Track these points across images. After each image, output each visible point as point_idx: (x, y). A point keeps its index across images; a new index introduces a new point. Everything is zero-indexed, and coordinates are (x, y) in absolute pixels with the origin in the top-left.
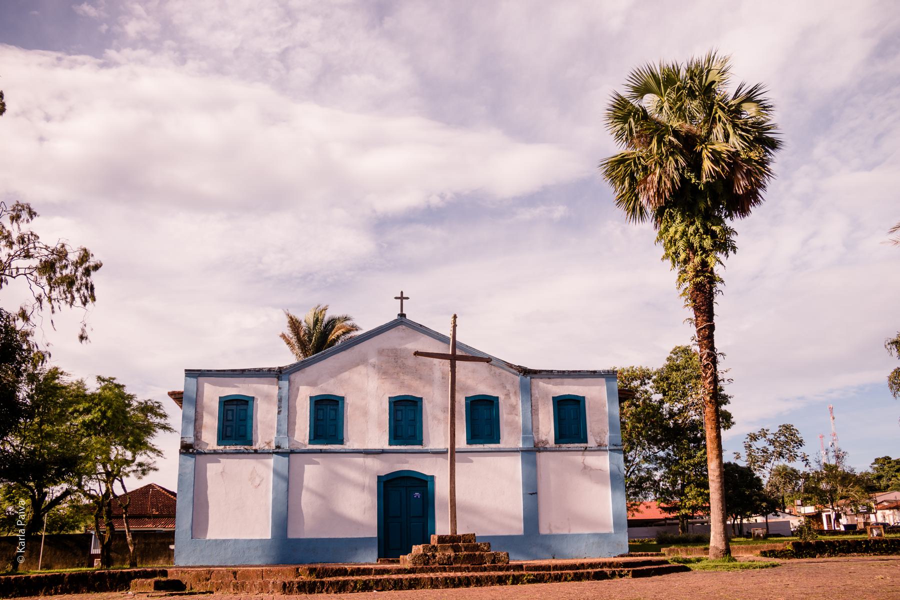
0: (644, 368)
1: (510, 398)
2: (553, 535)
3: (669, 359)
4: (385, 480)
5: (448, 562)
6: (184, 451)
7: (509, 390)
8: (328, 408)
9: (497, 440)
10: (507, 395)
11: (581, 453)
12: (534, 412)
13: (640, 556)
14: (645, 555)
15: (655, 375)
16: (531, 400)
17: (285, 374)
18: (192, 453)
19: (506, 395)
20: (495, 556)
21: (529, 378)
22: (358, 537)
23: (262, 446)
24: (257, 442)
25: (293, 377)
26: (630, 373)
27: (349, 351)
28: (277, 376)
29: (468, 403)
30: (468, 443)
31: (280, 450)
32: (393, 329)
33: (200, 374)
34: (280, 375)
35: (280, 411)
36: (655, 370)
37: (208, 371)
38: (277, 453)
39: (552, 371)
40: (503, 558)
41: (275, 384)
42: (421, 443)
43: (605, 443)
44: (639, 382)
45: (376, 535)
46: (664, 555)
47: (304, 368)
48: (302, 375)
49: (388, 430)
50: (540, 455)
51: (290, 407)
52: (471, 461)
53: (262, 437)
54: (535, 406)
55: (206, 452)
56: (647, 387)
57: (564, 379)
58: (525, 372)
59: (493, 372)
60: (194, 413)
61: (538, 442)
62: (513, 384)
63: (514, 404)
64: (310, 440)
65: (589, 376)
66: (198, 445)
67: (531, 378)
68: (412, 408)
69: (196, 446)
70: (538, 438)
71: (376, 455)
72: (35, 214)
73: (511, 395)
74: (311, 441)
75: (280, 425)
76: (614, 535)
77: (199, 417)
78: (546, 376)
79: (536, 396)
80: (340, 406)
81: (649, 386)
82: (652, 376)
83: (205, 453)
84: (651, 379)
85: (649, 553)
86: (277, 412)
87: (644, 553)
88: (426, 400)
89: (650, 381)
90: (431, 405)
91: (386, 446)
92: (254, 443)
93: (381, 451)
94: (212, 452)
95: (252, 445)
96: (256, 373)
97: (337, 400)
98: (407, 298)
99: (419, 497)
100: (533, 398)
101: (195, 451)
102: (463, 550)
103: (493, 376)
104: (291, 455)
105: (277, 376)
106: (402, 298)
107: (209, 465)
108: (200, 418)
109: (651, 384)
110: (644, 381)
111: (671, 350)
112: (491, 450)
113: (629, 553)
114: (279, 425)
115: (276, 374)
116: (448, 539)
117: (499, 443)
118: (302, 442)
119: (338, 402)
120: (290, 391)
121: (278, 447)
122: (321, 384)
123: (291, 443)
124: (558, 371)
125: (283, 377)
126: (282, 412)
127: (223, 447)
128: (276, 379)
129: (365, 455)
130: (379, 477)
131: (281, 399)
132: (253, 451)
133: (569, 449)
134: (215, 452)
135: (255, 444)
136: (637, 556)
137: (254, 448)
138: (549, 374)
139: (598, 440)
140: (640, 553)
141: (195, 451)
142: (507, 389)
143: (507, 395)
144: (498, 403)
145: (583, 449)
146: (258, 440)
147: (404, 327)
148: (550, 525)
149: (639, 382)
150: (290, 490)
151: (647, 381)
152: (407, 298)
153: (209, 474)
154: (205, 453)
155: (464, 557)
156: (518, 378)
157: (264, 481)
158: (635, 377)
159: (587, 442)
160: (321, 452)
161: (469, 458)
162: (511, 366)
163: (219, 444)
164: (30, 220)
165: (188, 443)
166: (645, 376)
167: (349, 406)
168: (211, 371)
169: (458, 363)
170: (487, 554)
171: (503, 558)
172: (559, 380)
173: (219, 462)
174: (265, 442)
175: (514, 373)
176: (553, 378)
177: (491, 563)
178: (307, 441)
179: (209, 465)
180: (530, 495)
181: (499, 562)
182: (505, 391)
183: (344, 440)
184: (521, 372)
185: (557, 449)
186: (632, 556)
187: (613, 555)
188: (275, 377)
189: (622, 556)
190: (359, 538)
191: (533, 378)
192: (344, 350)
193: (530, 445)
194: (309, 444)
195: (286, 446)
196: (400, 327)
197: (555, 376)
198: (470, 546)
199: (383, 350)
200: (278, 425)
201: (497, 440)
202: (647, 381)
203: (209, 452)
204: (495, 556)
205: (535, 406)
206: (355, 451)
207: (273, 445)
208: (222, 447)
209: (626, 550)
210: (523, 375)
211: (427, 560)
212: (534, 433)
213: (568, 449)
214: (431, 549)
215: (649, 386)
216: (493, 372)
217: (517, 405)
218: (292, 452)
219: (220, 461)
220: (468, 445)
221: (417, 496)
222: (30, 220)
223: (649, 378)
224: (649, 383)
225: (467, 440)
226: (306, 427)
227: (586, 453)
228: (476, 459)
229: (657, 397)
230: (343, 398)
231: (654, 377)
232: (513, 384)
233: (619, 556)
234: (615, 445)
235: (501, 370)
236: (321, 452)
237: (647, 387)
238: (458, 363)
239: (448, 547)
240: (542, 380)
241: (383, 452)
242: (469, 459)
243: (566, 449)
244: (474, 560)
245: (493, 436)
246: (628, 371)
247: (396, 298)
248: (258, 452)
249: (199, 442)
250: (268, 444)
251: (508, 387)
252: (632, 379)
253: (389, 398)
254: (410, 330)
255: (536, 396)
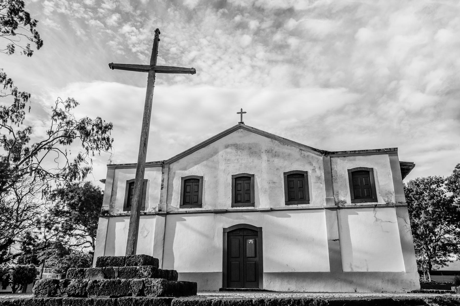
0: (438, 176)
1: (316, 172)
2: (354, 272)
3: (455, 171)
4: (228, 231)
5: (82, 292)
6: (102, 215)
7: (314, 166)
8: (193, 185)
9: (308, 202)
10: (314, 170)
11: (373, 209)
12: (334, 181)
13: (432, 292)
14: (436, 292)
15: (447, 180)
16: (332, 173)
17: (166, 164)
18: (107, 216)
19: (313, 170)
20: (144, 285)
21: (329, 157)
22: (209, 272)
23: (150, 211)
24: (148, 208)
25: (171, 166)
26: (429, 181)
27: (206, 147)
28: (162, 165)
29: (286, 176)
30: (286, 204)
31: (162, 212)
32: (235, 132)
33: (116, 167)
34: (164, 165)
35: (163, 187)
36: (445, 178)
37: (120, 165)
38: (158, 214)
39: (345, 152)
40: (155, 288)
41: (161, 171)
42: (253, 205)
43: (392, 202)
44: (436, 185)
45: (221, 271)
46: (454, 293)
47: (178, 160)
48: (177, 164)
49: (231, 197)
50: (340, 211)
51: (169, 185)
52: (290, 217)
53: (151, 204)
54: (334, 176)
55: (115, 215)
56: (442, 188)
57: (357, 157)
58: (325, 153)
59: (303, 155)
60: (111, 191)
61: (338, 202)
62: (317, 162)
63: (319, 176)
64: (180, 205)
65: (375, 153)
66: (112, 211)
67: (331, 157)
68: (301, 179)
69: (111, 212)
70: (338, 199)
71: (222, 214)
72: (78, 103)
73: (316, 169)
74: (181, 206)
75: (162, 197)
76: (406, 274)
77: (114, 193)
78: (342, 155)
79: (335, 169)
80: (305, 178)
81: (443, 188)
82: (444, 182)
83: (115, 216)
84: (443, 183)
85: (440, 291)
86: (161, 188)
87: (435, 290)
88: (257, 176)
89: (444, 184)
90: (260, 179)
91: (230, 208)
92: (145, 209)
93: (225, 211)
94: (119, 215)
95: (144, 210)
96: (149, 164)
97: (303, 174)
98: (245, 113)
99: (252, 243)
100: (333, 171)
101: (108, 215)
102: (116, 275)
103: (303, 158)
104: (168, 216)
105: (162, 165)
106: (242, 113)
107: (117, 223)
108: (115, 194)
109: (444, 186)
110: (439, 185)
111: (456, 166)
112: (302, 208)
113: (421, 289)
114: (162, 196)
115: (161, 164)
116: (109, 261)
117: (309, 203)
118: (176, 207)
119: (199, 180)
120: (169, 174)
121: (160, 210)
122: (189, 169)
123: (168, 208)
124: (350, 151)
125: (165, 166)
126: (164, 188)
127: (127, 211)
128: (161, 168)
129: (215, 214)
130: (224, 229)
131: (163, 180)
132: (143, 214)
133: (363, 206)
134: (121, 215)
135: (146, 209)
136: (428, 292)
137: (145, 211)
138: (344, 154)
139: (386, 199)
140: (431, 290)
141: (108, 215)
142: (314, 165)
143: (314, 170)
144: (308, 175)
145: (374, 206)
146: (148, 207)
147: (242, 130)
148: (351, 265)
149: (436, 185)
150: (166, 239)
151: (441, 185)
152: (245, 113)
153: (117, 229)
154: (115, 216)
155: (103, 286)
156: (321, 158)
157: (150, 233)
158: (432, 183)
159: (377, 201)
160: (186, 213)
161: (289, 214)
162: (315, 150)
163: (124, 210)
164: (75, 107)
165: (105, 210)
166: (439, 182)
167: (206, 182)
168: (122, 165)
169: (146, 62)
170: (134, 282)
171: (155, 288)
172: (352, 158)
173: (124, 221)
174: (153, 208)
175: (318, 155)
176: (348, 156)
177: (138, 296)
178: (178, 206)
179: (117, 223)
180: (334, 241)
181: (148, 293)
182: (312, 167)
183: (202, 205)
184: (323, 154)
185: (353, 206)
186: (424, 292)
187: (407, 291)
188: (161, 166)
189: (415, 292)
190: (210, 273)
191: (333, 157)
192: (204, 147)
193: (332, 205)
194: (180, 208)
195: (165, 210)
196: (240, 130)
197: (349, 155)
198: (126, 271)
199: (229, 145)
200: (161, 197)
201: (308, 202)
202: (441, 185)
203: (117, 215)
204: (144, 285)
205: (334, 176)
206: (208, 211)
207: (157, 210)
208: (126, 212)
209: (418, 287)
210: (325, 156)
211: (54, 289)
212: (334, 196)
213: (361, 206)
214: (77, 274)
215: (443, 188)
216: (303, 155)
217: (321, 176)
218: (168, 213)
219: (124, 220)
220: (287, 206)
221: (251, 242)
222: (75, 107)
223: (442, 183)
224: (442, 186)
225: (285, 202)
226: (178, 197)
227: (377, 209)
228: (292, 214)
229: (449, 194)
230: (202, 177)
231: (446, 182)
232: (317, 162)
233: (412, 292)
234: (401, 203)
235: (309, 153)
236: (186, 213)
237: (442, 188)
238: (146, 62)
239: (99, 273)
240: (339, 158)
241: (226, 212)
242: (288, 215)
243: (360, 206)
244: (116, 289)
245: (305, 199)
246: (428, 180)
247: (238, 113)
248: (147, 214)
249: (113, 209)
250: (154, 209)
251: (314, 164)
252: (431, 184)
253: (232, 176)
254: (246, 131)
255: (335, 169)
